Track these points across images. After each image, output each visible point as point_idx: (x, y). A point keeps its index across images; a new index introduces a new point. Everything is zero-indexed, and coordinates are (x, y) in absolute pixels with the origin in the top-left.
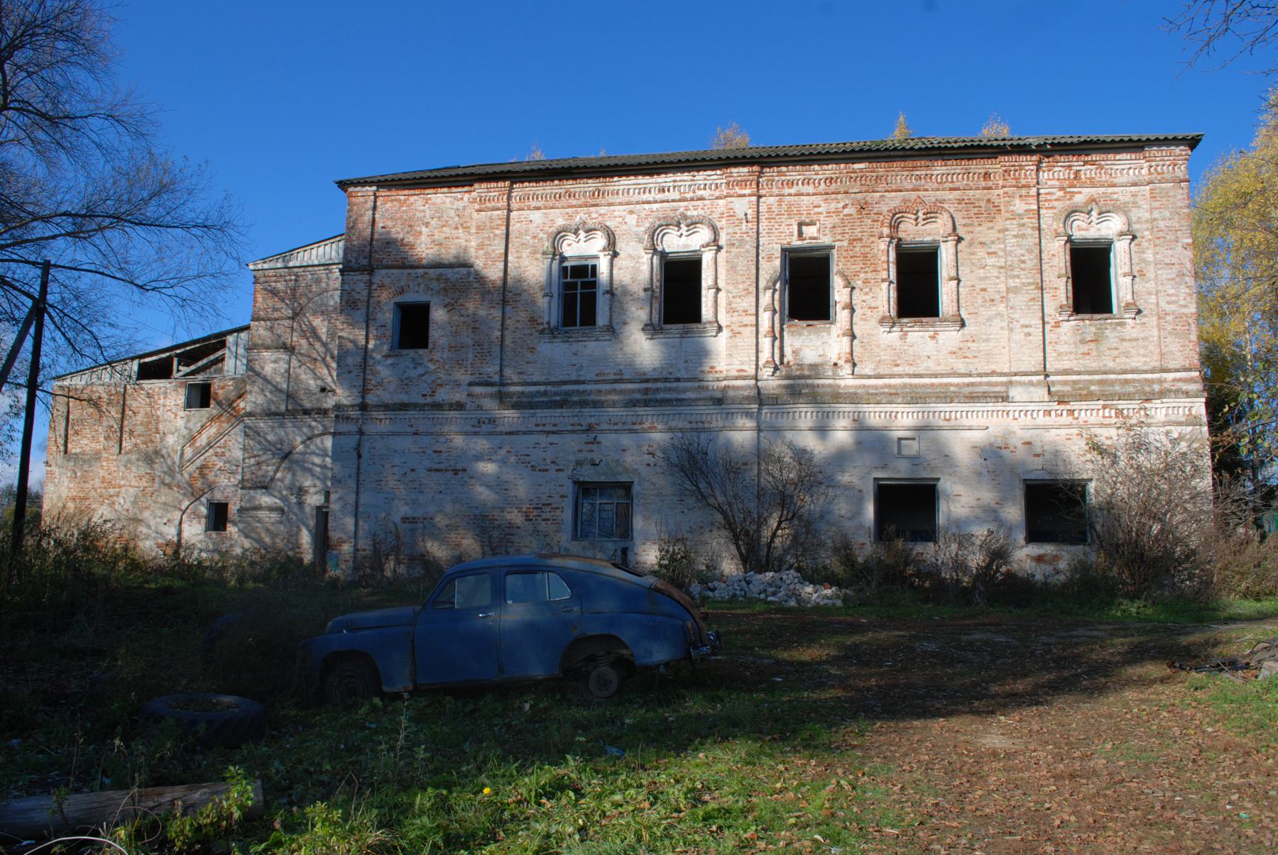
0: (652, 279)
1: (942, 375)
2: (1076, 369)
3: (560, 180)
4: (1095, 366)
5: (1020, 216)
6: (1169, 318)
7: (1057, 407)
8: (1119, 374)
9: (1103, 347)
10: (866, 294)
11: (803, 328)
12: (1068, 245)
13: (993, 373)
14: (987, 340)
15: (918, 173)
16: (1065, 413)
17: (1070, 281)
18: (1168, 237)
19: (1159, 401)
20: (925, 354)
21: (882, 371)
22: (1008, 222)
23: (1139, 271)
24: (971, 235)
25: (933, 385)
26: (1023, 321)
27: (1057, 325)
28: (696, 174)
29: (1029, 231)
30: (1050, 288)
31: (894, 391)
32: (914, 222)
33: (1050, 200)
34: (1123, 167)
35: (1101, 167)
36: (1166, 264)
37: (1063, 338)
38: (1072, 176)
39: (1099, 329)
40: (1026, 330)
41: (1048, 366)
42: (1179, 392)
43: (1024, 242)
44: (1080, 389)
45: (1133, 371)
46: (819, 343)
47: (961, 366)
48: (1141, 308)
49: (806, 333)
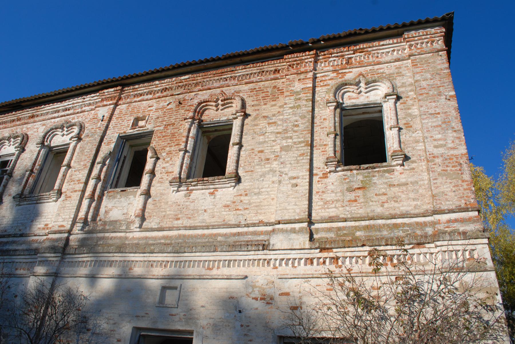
0: (34, 164)
1: (214, 227)
2: (342, 216)
3: (15, 112)
4: (362, 212)
5: (298, 93)
6: (439, 160)
7: (320, 255)
8: (388, 218)
9: (371, 193)
10: (167, 162)
11: (118, 193)
12: (338, 110)
13: (261, 223)
14: (259, 193)
15: (225, 76)
16: (328, 261)
17: (338, 137)
18: (431, 93)
19: (432, 245)
20: (203, 208)
21: (166, 224)
22: (287, 98)
23: (405, 124)
24: (257, 112)
25: (204, 235)
26: (292, 174)
27: (325, 176)
28: (85, 97)
29: (304, 102)
30: (320, 145)
31: (169, 242)
32: (215, 108)
33: (326, 80)
34: (387, 50)
35: (369, 53)
36: (431, 114)
37: (331, 187)
38: (344, 62)
39: (366, 177)
40: (294, 181)
41: (314, 215)
42: (453, 235)
43: (299, 111)
44: (345, 235)
45: (403, 216)
46: (126, 204)
47: (231, 218)
48: (409, 155)
49: (119, 196)
